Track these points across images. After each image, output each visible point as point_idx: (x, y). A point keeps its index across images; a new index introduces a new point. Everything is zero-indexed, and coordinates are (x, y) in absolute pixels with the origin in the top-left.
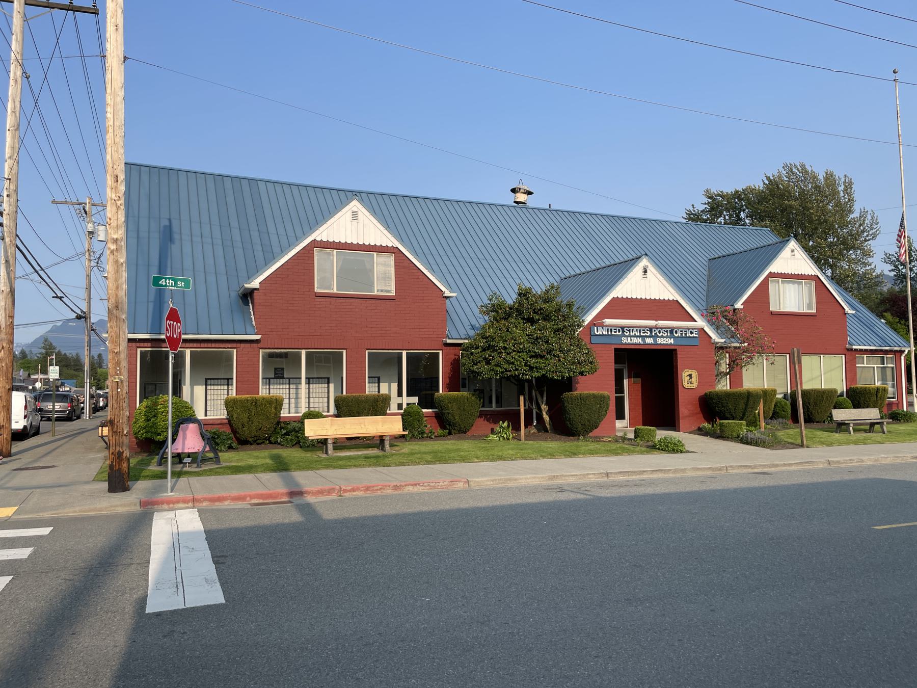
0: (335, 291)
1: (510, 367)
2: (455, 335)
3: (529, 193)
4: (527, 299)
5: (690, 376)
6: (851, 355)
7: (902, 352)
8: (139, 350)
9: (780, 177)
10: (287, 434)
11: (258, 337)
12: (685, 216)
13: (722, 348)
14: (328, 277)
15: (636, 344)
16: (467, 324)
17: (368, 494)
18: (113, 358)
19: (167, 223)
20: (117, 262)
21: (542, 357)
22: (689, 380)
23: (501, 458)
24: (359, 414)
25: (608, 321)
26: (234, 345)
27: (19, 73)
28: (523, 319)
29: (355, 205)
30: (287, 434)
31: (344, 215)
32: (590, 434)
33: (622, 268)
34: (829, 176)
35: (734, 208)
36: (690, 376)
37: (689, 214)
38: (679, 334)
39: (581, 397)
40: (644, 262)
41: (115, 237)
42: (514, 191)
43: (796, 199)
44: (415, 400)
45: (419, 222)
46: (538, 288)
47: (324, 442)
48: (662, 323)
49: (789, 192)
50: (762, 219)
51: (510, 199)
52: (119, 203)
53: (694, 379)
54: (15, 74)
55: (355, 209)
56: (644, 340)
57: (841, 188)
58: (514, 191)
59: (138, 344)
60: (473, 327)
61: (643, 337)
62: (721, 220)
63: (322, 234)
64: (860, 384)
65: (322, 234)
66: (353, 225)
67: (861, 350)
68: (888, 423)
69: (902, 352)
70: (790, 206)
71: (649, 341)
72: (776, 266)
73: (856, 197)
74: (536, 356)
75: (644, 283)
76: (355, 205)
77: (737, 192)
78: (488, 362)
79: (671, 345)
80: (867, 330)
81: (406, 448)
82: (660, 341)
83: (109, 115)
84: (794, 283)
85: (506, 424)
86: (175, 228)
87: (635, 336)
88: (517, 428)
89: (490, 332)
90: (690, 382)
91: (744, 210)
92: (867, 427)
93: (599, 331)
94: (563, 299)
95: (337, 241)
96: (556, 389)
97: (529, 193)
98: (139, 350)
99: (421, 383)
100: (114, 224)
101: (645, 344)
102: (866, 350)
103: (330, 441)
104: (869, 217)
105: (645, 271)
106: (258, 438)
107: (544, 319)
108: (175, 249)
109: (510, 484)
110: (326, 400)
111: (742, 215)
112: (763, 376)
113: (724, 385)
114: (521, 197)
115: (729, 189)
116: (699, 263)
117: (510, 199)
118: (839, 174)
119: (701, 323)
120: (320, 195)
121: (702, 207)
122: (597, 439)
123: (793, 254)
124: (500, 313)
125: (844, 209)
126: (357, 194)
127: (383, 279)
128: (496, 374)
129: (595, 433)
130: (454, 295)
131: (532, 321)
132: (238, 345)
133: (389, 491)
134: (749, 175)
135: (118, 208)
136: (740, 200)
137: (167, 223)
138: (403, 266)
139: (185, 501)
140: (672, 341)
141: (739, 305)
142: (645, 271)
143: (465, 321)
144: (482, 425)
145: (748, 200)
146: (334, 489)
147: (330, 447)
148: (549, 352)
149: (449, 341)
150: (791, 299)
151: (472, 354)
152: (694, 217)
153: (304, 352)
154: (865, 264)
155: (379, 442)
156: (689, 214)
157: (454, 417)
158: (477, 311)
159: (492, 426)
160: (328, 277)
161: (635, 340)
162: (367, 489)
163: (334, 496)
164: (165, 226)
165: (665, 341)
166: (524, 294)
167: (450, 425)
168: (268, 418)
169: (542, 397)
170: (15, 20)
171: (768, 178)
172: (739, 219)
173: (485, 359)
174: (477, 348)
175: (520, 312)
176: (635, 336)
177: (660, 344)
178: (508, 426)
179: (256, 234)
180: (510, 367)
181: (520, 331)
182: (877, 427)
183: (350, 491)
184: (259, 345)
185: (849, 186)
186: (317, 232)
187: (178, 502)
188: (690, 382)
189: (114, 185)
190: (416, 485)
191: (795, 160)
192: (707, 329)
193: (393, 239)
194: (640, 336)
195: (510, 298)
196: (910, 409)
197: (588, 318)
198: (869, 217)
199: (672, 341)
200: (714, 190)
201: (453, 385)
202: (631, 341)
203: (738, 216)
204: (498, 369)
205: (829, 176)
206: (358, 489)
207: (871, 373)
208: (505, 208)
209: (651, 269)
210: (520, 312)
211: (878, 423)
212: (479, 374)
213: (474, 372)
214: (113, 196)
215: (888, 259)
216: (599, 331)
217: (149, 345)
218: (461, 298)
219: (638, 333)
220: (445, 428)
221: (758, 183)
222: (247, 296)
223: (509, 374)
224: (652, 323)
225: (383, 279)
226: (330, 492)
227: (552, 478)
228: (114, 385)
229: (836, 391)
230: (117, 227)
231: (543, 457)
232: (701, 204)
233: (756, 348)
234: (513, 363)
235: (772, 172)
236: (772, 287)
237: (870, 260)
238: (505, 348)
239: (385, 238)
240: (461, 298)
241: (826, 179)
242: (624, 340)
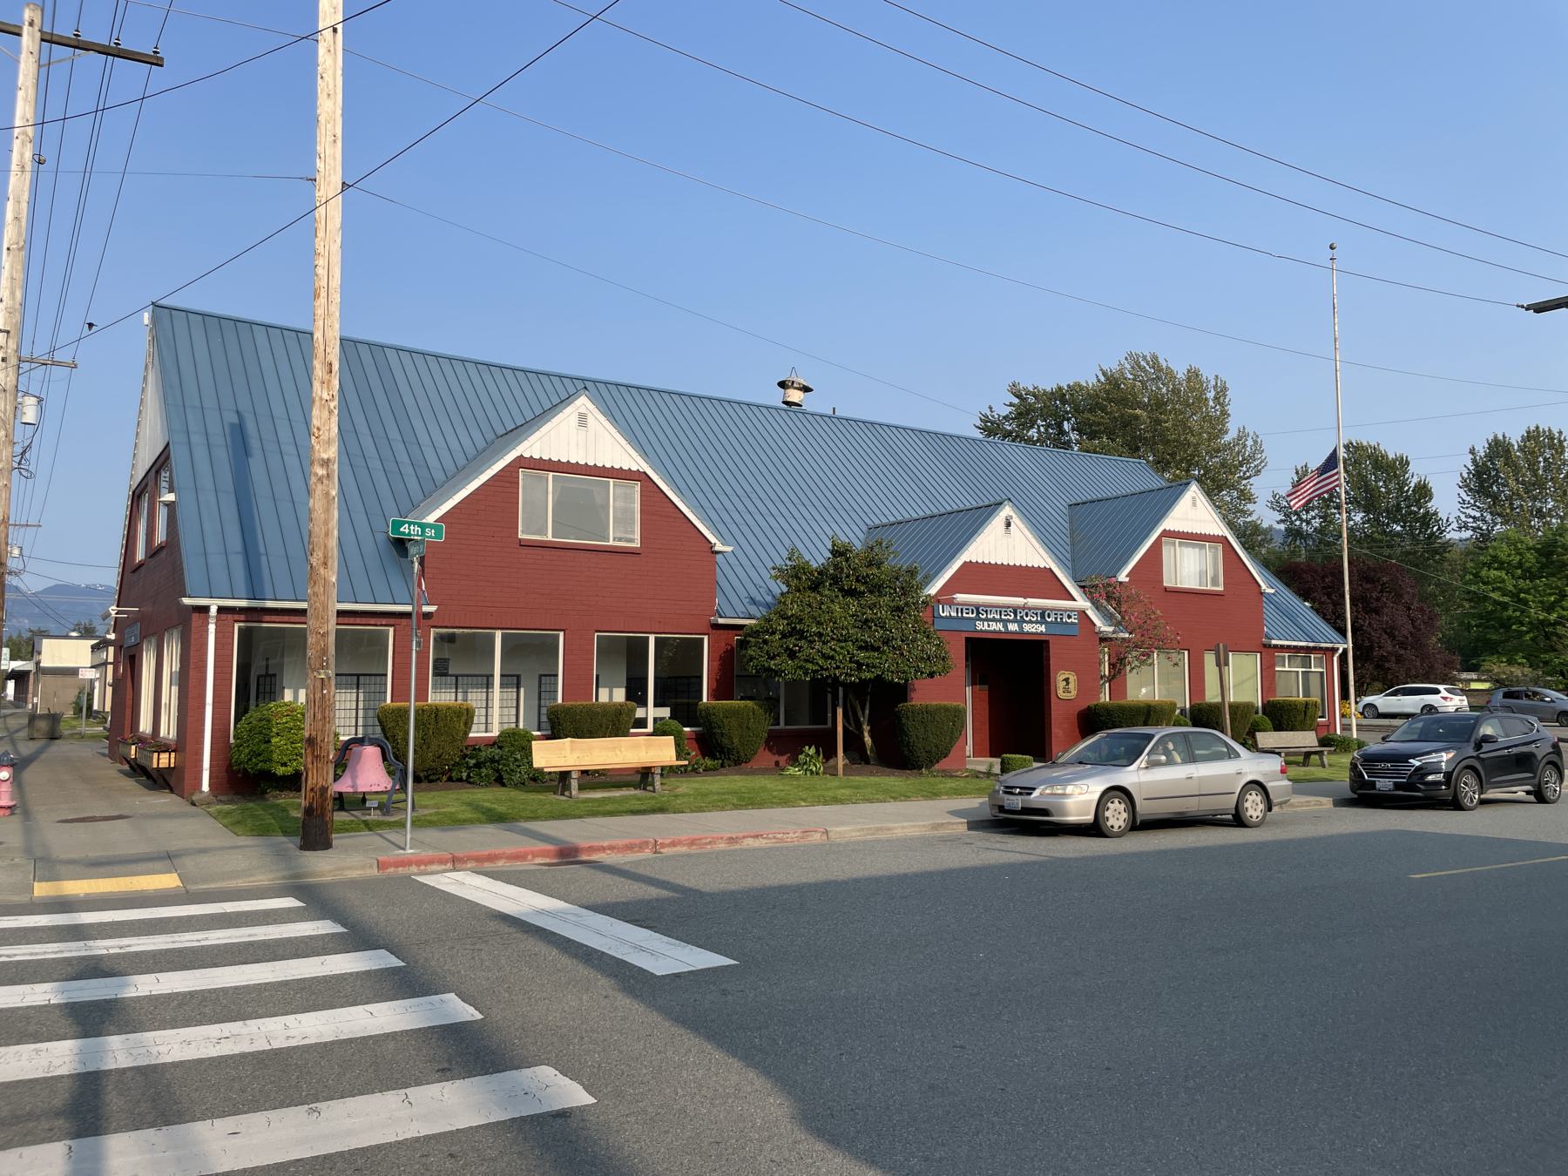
0: (550, 538)
1: (827, 664)
2: (728, 611)
3: (806, 389)
4: (847, 560)
5: (1067, 680)
6: (1269, 652)
7: (1334, 650)
8: (236, 626)
9: (1121, 372)
10: (478, 765)
11: (432, 609)
12: (979, 423)
13: (1103, 640)
14: (540, 517)
15: (995, 632)
16: (743, 594)
17: (694, 850)
18: (318, 642)
19: (235, 420)
20: (327, 494)
21: (877, 649)
22: (1065, 686)
23: (836, 800)
24: (591, 735)
25: (960, 597)
26: (392, 621)
27: (28, 155)
28: (842, 590)
29: (583, 403)
30: (478, 765)
31: (565, 420)
32: (937, 767)
33: (974, 519)
34: (1193, 375)
35: (1055, 415)
36: (1067, 680)
37: (985, 419)
38: (1051, 619)
39: (927, 711)
40: (1007, 511)
41: (325, 456)
42: (782, 385)
43: (1144, 407)
44: (665, 712)
45: (657, 428)
46: (856, 539)
47: (564, 776)
48: (1032, 602)
49: (1135, 395)
50: (1093, 436)
51: (775, 397)
52: (332, 405)
53: (1072, 686)
54: (22, 155)
55: (583, 410)
56: (1005, 626)
57: (1211, 395)
58: (782, 385)
59: (236, 617)
60: (753, 601)
61: (1006, 622)
62: (1033, 433)
63: (534, 446)
64: (1279, 697)
65: (534, 446)
66: (579, 435)
67: (1282, 647)
68: (1330, 753)
69: (1334, 650)
70: (1137, 417)
71: (1013, 627)
72: (1171, 522)
73: (1230, 409)
74: (866, 647)
75: (1007, 542)
76: (583, 403)
77: (1060, 389)
78: (792, 655)
79: (1041, 634)
80: (1291, 619)
81: (686, 786)
82: (1027, 628)
83: (321, 271)
84: (1194, 546)
85: (812, 751)
86: (250, 426)
87: (994, 620)
88: (830, 753)
89: (794, 609)
90: (1067, 690)
91: (1068, 420)
92: (1301, 759)
93: (945, 611)
94: (896, 561)
95: (555, 459)
96: (884, 699)
97: (806, 389)
98: (236, 626)
99: (677, 690)
100: (324, 437)
101: (1007, 632)
102: (1289, 647)
103: (574, 775)
104: (1250, 442)
105: (1008, 525)
106: (434, 771)
107: (871, 592)
108: (256, 464)
109: (882, 836)
110: (513, 711)
111: (1066, 426)
112: (1150, 684)
113: (1105, 698)
114: (795, 396)
115: (1048, 385)
116: (1057, 509)
117: (775, 397)
118: (1207, 374)
119: (1081, 602)
120: (487, 377)
121: (1005, 411)
122: (948, 774)
123: (1194, 504)
124: (801, 578)
125: (1217, 424)
126: (585, 385)
127: (622, 527)
128: (806, 674)
129: (943, 764)
130: (729, 549)
131: (851, 593)
132: (397, 621)
133: (722, 846)
134: (1079, 367)
135: (330, 412)
136: (1064, 402)
137: (235, 420)
138: (655, 504)
139: (441, 861)
140: (1042, 628)
141: (1123, 577)
142: (1008, 525)
143: (745, 588)
144: (766, 758)
145: (1073, 402)
146: (647, 843)
147: (574, 784)
148: (886, 642)
149: (721, 621)
150: (1189, 569)
151: (765, 642)
152: (991, 428)
153: (498, 634)
154: (1243, 512)
155: (644, 776)
156: (985, 419)
157: (731, 738)
158: (766, 576)
159: (776, 758)
160: (540, 517)
161: (995, 626)
162: (692, 843)
163: (647, 854)
164: (232, 425)
165: (1034, 629)
166: (839, 552)
167: (722, 752)
168: (454, 740)
169: (863, 710)
170: (22, 66)
171: (1104, 374)
172: (1062, 432)
173: (787, 648)
174: (773, 633)
175: (835, 580)
176: (994, 620)
177: (1028, 633)
178: (817, 752)
179: (401, 446)
180: (827, 664)
181: (842, 610)
182: (1314, 758)
183: (669, 845)
184: (430, 622)
185: (1221, 392)
186: (525, 444)
187: (431, 862)
188: (1067, 690)
189: (326, 377)
190: (757, 836)
191: (1145, 349)
192: (1090, 613)
193: (639, 459)
194: (1001, 620)
195: (818, 557)
196: (1346, 734)
197: (933, 589)
198: (1250, 442)
199: (1042, 628)
200: (1027, 384)
201: (722, 690)
202: (989, 627)
203: (1060, 426)
204: (809, 666)
205: (1193, 375)
206: (680, 843)
207: (1294, 681)
208: (666, 396)
209: (1016, 521)
210: (835, 580)
211: (1315, 753)
212: (777, 673)
213: (769, 669)
214: (325, 396)
215: (1276, 504)
216: (945, 611)
217: (242, 617)
218: (739, 553)
219: (999, 616)
220: (714, 758)
221: (1088, 376)
222: (401, 545)
223: (825, 674)
224: (1019, 601)
225: (622, 527)
226: (642, 846)
227: (936, 827)
228: (318, 684)
229: (1174, 705)
230: (329, 442)
231: (895, 799)
232: (1002, 406)
233: (1147, 641)
234: (832, 658)
235: (1112, 365)
236: (1167, 552)
237: (1250, 507)
238: (820, 635)
239: (630, 459)
240: (739, 553)
241: (1189, 380)
242: (980, 626)
